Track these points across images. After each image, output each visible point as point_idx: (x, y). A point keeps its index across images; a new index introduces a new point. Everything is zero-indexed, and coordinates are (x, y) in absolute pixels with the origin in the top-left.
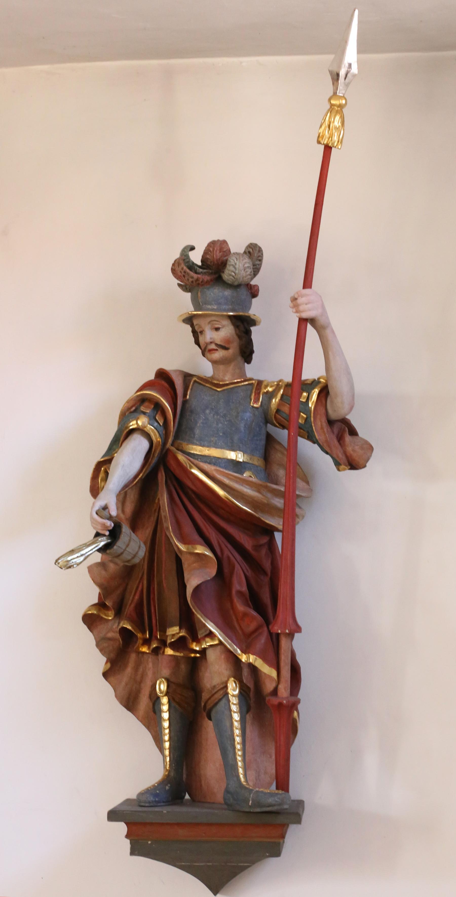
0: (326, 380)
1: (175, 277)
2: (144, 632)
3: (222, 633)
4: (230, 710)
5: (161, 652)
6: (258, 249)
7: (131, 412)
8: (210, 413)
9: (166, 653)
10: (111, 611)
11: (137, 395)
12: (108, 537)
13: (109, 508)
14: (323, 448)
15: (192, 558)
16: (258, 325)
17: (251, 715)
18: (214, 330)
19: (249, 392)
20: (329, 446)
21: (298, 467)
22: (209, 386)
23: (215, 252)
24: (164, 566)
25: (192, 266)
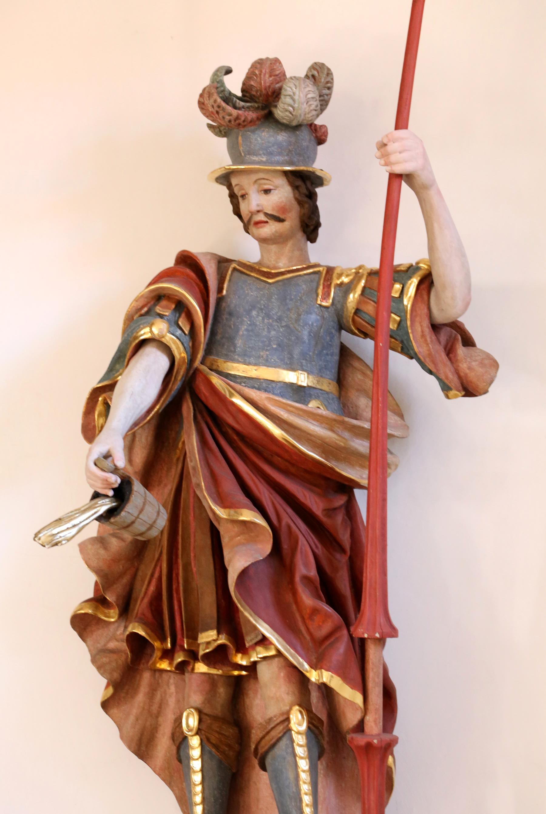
0: (428, 265)
1: (204, 114)
2: (163, 640)
3: (280, 639)
4: (294, 755)
5: (190, 668)
6: (325, 72)
7: (141, 315)
8: (258, 316)
9: (196, 671)
10: (114, 608)
11: (151, 290)
12: (113, 499)
13: (113, 455)
14: (426, 366)
15: (237, 529)
16: (326, 185)
17: (324, 763)
18: (262, 192)
19: (315, 284)
20: (434, 362)
21: (388, 394)
22: (256, 275)
23: (262, 76)
24: (192, 540)
25: (228, 98)
